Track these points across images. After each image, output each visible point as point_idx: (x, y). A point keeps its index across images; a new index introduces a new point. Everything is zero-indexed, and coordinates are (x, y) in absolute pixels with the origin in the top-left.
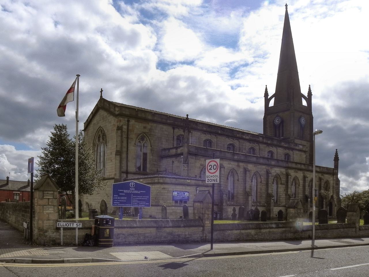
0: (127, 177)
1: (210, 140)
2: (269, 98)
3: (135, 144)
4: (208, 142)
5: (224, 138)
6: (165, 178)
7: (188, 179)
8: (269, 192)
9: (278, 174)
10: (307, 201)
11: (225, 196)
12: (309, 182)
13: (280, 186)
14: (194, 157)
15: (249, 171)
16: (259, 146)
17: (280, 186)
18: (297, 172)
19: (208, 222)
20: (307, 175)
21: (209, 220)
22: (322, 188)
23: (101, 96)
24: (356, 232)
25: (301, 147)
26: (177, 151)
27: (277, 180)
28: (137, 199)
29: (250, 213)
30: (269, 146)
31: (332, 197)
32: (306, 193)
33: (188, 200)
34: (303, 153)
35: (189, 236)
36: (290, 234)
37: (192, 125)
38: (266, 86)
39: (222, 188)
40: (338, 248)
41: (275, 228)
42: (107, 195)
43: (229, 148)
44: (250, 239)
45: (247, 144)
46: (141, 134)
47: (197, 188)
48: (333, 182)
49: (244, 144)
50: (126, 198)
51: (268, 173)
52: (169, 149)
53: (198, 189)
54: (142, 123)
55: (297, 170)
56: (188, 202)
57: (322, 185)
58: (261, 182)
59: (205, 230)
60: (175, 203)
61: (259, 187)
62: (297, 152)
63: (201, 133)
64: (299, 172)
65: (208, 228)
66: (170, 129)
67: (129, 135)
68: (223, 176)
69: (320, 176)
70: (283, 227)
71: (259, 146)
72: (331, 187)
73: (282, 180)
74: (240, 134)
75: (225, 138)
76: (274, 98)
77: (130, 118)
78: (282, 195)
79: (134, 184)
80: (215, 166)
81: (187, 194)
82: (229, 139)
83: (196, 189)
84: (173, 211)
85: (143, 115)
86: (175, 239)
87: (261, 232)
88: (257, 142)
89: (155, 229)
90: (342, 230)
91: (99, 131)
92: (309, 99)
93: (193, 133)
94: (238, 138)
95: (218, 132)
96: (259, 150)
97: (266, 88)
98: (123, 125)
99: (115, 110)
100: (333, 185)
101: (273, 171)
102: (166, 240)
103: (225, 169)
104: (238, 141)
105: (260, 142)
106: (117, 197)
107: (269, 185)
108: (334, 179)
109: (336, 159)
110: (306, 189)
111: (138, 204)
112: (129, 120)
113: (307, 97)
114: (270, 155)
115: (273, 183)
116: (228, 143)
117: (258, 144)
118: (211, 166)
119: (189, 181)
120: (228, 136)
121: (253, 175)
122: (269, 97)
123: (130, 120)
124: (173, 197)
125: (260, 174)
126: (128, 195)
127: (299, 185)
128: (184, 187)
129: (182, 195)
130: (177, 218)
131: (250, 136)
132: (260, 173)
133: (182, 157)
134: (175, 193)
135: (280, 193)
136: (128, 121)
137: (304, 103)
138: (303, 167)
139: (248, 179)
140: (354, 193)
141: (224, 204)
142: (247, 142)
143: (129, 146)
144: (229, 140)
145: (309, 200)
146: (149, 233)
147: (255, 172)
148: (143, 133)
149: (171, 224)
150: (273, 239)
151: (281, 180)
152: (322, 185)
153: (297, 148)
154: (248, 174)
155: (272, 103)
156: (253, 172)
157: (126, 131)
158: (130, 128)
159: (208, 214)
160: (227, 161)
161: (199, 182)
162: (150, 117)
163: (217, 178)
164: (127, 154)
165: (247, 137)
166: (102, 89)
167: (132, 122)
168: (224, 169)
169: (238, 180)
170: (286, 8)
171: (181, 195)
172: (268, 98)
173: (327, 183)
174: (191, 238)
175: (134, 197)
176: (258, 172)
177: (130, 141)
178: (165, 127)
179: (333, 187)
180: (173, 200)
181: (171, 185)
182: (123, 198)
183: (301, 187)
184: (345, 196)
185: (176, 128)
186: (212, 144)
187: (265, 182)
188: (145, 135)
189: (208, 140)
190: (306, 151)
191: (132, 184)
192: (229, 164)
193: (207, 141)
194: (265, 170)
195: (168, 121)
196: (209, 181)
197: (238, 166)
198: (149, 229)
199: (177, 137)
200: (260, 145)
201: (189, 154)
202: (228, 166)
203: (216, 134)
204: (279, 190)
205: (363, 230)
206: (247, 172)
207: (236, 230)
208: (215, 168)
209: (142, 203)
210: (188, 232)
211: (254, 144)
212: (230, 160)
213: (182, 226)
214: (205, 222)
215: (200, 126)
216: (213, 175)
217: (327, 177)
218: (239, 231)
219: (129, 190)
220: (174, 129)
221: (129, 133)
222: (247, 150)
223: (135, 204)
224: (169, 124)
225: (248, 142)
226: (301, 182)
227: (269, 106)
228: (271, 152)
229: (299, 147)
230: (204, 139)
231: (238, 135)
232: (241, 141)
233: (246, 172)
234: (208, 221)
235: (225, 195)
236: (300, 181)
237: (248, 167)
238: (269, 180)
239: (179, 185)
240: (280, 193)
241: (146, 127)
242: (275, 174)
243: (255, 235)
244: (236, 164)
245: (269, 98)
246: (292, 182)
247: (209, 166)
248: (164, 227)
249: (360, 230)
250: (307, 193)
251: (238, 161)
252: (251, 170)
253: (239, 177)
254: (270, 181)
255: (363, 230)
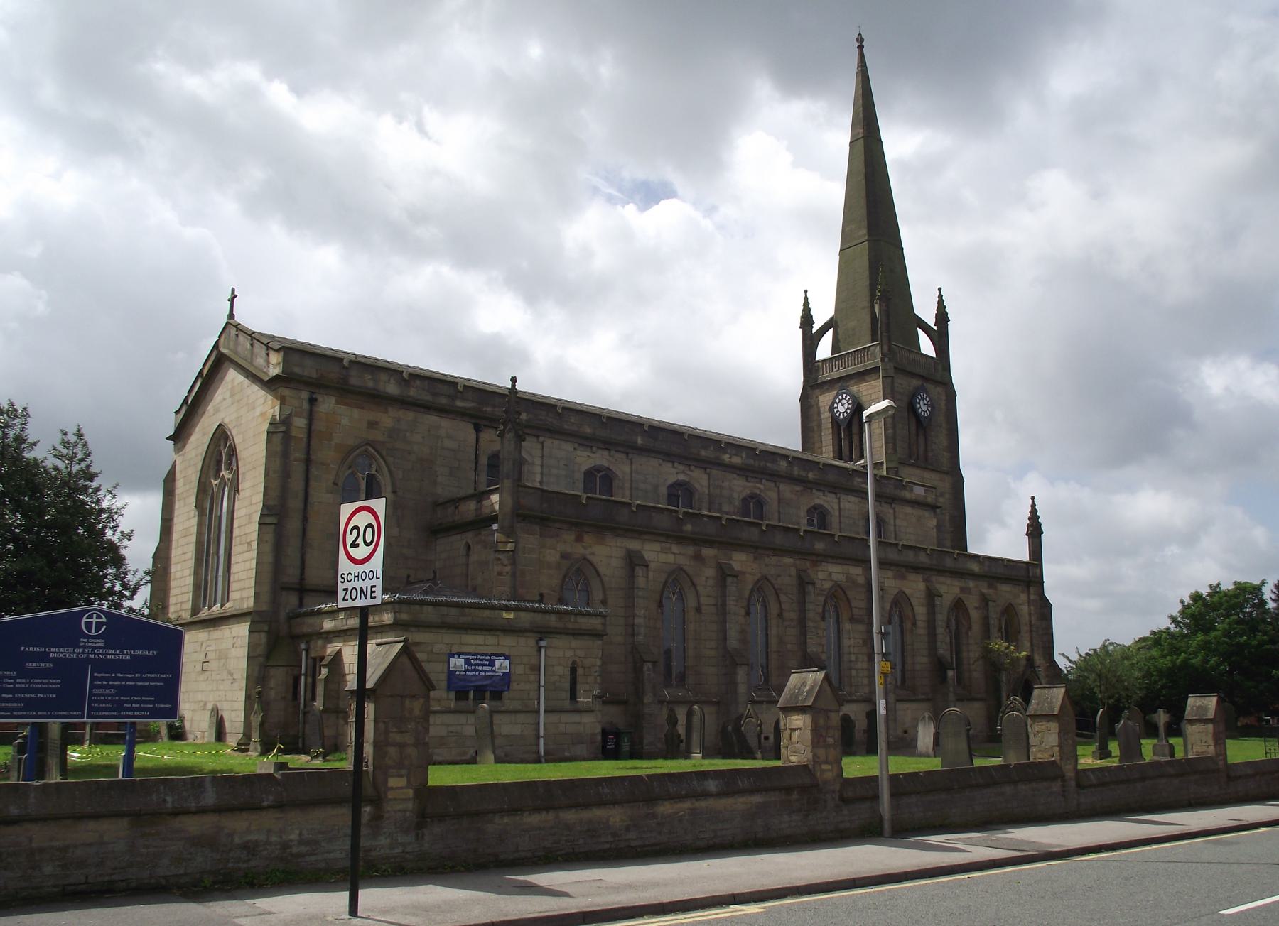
0: (301, 605)
1: (608, 469)
2: (814, 330)
3: (335, 484)
4: (599, 475)
5: (654, 462)
6: (417, 607)
7: (507, 609)
8: (808, 650)
9: (839, 586)
10: (944, 679)
11: (649, 670)
12: (949, 613)
13: (847, 626)
14: (537, 528)
15: (736, 576)
16: (776, 489)
17: (847, 626)
18: (903, 578)
19: (402, 782)
20: (938, 586)
21: (404, 772)
22: (994, 631)
23: (231, 316)
24: (1064, 796)
25: (919, 491)
26: (481, 508)
27: (836, 607)
28: (112, 687)
29: (730, 728)
30: (811, 489)
31: (1029, 659)
32: (941, 652)
33: (506, 688)
34: (927, 514)
35: (304, 849)
36: (786, 818)
37: (543, 418)
38: (806, 292)
39: (641, 637)
40: (966, 876)
41: (720, 795)
42: (232, 675)
43: (672, 497)
44: (607, 846)
45: (735, 482)
46: (358, 447)
47: (541, 639)
48: (1030, 610)
49: (726, 484)
50: (55, 683)
51: (803, 583)
52: (456, 501)
53: (543, 643)
54: (363, 408)
55: (903, 570)
56: (506, 693)
57: (994, 621)
58: (780, 615)
59: (386, 815)
60: (457, 699)
61: (774, 631)
62: (908, 510)
63: (576, 445)
64: (912, 576)
65: (400, 807)
66: (466, 431)
67: (311, 452)
68: (640, 594)
69: (985, 591)
70: (751, 792)
71: (779, 487)
72: (1025, 629)
73: (853, 605)
74: (712, 448)
75: (661, 461)
76: (829, 334)
77: (317, 391)
78: (857, 658)
79: (104, 620)
80: (369, 530)
81: (502, 665)
82: (673, 467)
83: (537, 643)
84: (451, 729)
85: (368, 381)
86: (230, 865)
87: (654, 816)
88: (771, 475)
89: (124, 823)
90: (1008, 789)
91: (219, 439)
92: (940, 336)
93: (545, 444)
94: (705, 464)
95: (637, 442)
96: (779, 503)
97: (806, 298)
98: (290, 415)
99: (268, 362)
100: (1031, 621)
101: (821, 575)
102: (182, 871)
103: (648, 571)
104: (705, 473)
105: (781, 477)
106: (10, 678)
107: (810, 624)
108: (1032, 597)
109: (1035, 530)
110: (940, 637)
111: (118, 706)
112: (314, 396)
113: (935, 328)
114: (816, 521)
115: (823, 619)
116: (671, 480)
117: (773, 484)
118: (355, 532)
119: (511, 615)
120: (669, 457)
121: (752, 591)
122: (815, 328)
123: (320, 399)
124: (451, 674)
125: (776, 587)
126: (71, 673)
127: (914, 624)
128: (491, 639)
129: (485, 668)
130: (464, 758)
131: (744, 455)
132: (774, 582)
133: (495, 527)
134: (457, 663)
135: (850, 653)
136: (312, 401)
137: (927, 347)
138: (923, 559)
139: (732, 603)
140: (1104, 647)
141: (648, 699)
142: (735, 476)
143: (311, 491)
144: (675, 471)
145: (950, 673)
146: (90, 845)
147: (759, 581)
148: (367, 444)
149: (209, 798)
150: (711, 842)
151: (851, 608)
152: (992, 622)
153: (907, 495)
154: (732, 588)
155: (824, 349)
156: (750, 580)
157: (303, 435)
158: (319, 426)
159: (402, 746)
160: (858, 566)
161: (547, 617)
162: (392, 388)
163: (374, 582)
164: (305, 519)
165: (737, 460)
166: (233, 290)
167: (327, 404)
168: (645, 568)
169: (698, 610)
170: (861, 47)
171: (480, 668)
172: (813, 332)
173: (1009, 611)
174: (313, 858)
175: (101, 679)
176: (770, 578)
177: (316, 473)
178: (445, 424)
179: (1031, 625)
180: (449, 688)
181: (444, 631)
182: (40, 683)
183: (922, 630)
184: (1078, 657)
185: (485, 426)
186: (616, 483)
187: (794, 615)
188: (373, 451)
189: (599, 471)
190: (939, 505)
191: (94, 620)
192: (663, 551)
193: (749, 499)
194: (793, 572)
195: (459, 403)
196: (348, 597)
197: (698, 557)
198: (92, 825)
199: (489, 458)
200: (782, 487)
201: (518, 515)
202: (663, 557)
203: (630, 449)
204: (846, 642)
205: (1091, 786)
206: (729, 580)
207: (537, 810)
208: (368, 540)
209: (136, 702)
210: (297, 832)
211: (761, 483)
212: (668, 536)
213: (265, 804)
214: (386, 782)
215: (572, 421)
216: (361, 568)
217: (1005, 591)
218: (551, 816)
219: (76, 645)
220: (478, 429)
221: (312, 443)
222: (737, 504)
223: (106, 709)
224: (463, 414)
225: (738, 475)
226: (921, 611)
227: (818, 358)
228: (819, 513)
229: (912, 490)
230: (584, 468)
231: (703, 453)
232: (715, 472)
233: (633, 570)
234: (401, 776)
235: (650, 665)
236: (916, 608)
237: (731, 562)
238: (809, 606)
239: (472, 629)
240: (850, 653)
241: (377, 423)
242: (827, 585)
243: (628, 829)
244: (690, 550)
245: (814, 330)
246: (890, 611)
247: (351, 533)
248: (176, 813)
249: (1079, 785)
250: (943, 650)
251: (697, 541)
252: (744, 573)
253: (703, 600)
254: (814, 608)
255: (1091, 786)
